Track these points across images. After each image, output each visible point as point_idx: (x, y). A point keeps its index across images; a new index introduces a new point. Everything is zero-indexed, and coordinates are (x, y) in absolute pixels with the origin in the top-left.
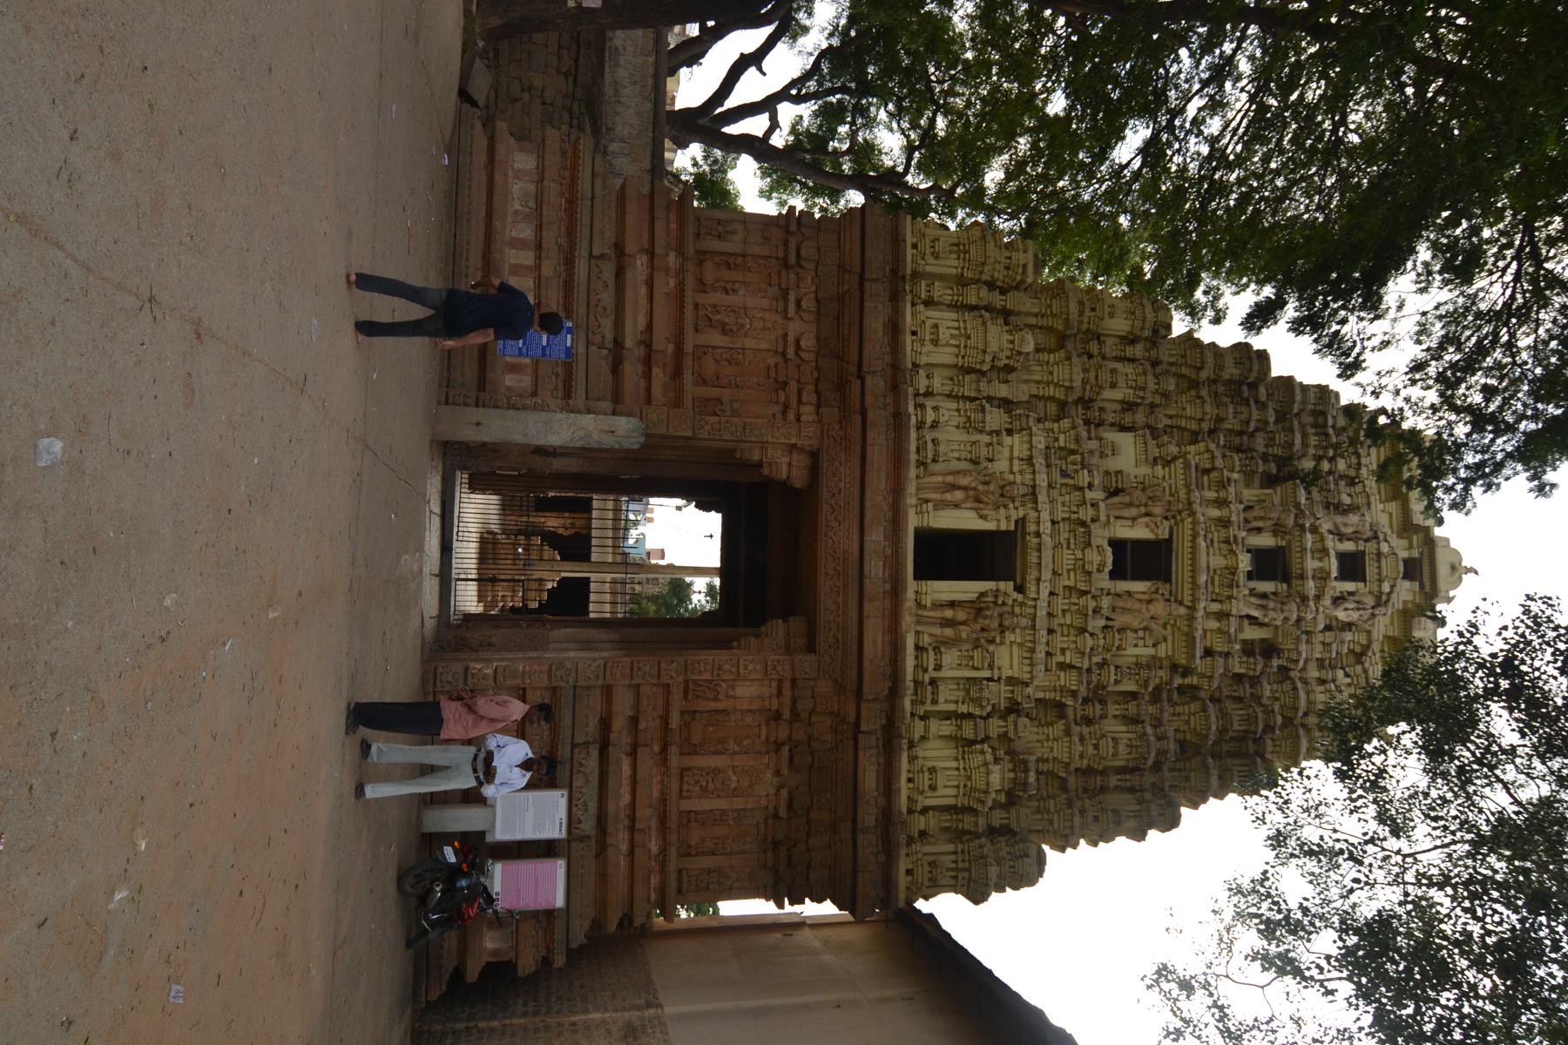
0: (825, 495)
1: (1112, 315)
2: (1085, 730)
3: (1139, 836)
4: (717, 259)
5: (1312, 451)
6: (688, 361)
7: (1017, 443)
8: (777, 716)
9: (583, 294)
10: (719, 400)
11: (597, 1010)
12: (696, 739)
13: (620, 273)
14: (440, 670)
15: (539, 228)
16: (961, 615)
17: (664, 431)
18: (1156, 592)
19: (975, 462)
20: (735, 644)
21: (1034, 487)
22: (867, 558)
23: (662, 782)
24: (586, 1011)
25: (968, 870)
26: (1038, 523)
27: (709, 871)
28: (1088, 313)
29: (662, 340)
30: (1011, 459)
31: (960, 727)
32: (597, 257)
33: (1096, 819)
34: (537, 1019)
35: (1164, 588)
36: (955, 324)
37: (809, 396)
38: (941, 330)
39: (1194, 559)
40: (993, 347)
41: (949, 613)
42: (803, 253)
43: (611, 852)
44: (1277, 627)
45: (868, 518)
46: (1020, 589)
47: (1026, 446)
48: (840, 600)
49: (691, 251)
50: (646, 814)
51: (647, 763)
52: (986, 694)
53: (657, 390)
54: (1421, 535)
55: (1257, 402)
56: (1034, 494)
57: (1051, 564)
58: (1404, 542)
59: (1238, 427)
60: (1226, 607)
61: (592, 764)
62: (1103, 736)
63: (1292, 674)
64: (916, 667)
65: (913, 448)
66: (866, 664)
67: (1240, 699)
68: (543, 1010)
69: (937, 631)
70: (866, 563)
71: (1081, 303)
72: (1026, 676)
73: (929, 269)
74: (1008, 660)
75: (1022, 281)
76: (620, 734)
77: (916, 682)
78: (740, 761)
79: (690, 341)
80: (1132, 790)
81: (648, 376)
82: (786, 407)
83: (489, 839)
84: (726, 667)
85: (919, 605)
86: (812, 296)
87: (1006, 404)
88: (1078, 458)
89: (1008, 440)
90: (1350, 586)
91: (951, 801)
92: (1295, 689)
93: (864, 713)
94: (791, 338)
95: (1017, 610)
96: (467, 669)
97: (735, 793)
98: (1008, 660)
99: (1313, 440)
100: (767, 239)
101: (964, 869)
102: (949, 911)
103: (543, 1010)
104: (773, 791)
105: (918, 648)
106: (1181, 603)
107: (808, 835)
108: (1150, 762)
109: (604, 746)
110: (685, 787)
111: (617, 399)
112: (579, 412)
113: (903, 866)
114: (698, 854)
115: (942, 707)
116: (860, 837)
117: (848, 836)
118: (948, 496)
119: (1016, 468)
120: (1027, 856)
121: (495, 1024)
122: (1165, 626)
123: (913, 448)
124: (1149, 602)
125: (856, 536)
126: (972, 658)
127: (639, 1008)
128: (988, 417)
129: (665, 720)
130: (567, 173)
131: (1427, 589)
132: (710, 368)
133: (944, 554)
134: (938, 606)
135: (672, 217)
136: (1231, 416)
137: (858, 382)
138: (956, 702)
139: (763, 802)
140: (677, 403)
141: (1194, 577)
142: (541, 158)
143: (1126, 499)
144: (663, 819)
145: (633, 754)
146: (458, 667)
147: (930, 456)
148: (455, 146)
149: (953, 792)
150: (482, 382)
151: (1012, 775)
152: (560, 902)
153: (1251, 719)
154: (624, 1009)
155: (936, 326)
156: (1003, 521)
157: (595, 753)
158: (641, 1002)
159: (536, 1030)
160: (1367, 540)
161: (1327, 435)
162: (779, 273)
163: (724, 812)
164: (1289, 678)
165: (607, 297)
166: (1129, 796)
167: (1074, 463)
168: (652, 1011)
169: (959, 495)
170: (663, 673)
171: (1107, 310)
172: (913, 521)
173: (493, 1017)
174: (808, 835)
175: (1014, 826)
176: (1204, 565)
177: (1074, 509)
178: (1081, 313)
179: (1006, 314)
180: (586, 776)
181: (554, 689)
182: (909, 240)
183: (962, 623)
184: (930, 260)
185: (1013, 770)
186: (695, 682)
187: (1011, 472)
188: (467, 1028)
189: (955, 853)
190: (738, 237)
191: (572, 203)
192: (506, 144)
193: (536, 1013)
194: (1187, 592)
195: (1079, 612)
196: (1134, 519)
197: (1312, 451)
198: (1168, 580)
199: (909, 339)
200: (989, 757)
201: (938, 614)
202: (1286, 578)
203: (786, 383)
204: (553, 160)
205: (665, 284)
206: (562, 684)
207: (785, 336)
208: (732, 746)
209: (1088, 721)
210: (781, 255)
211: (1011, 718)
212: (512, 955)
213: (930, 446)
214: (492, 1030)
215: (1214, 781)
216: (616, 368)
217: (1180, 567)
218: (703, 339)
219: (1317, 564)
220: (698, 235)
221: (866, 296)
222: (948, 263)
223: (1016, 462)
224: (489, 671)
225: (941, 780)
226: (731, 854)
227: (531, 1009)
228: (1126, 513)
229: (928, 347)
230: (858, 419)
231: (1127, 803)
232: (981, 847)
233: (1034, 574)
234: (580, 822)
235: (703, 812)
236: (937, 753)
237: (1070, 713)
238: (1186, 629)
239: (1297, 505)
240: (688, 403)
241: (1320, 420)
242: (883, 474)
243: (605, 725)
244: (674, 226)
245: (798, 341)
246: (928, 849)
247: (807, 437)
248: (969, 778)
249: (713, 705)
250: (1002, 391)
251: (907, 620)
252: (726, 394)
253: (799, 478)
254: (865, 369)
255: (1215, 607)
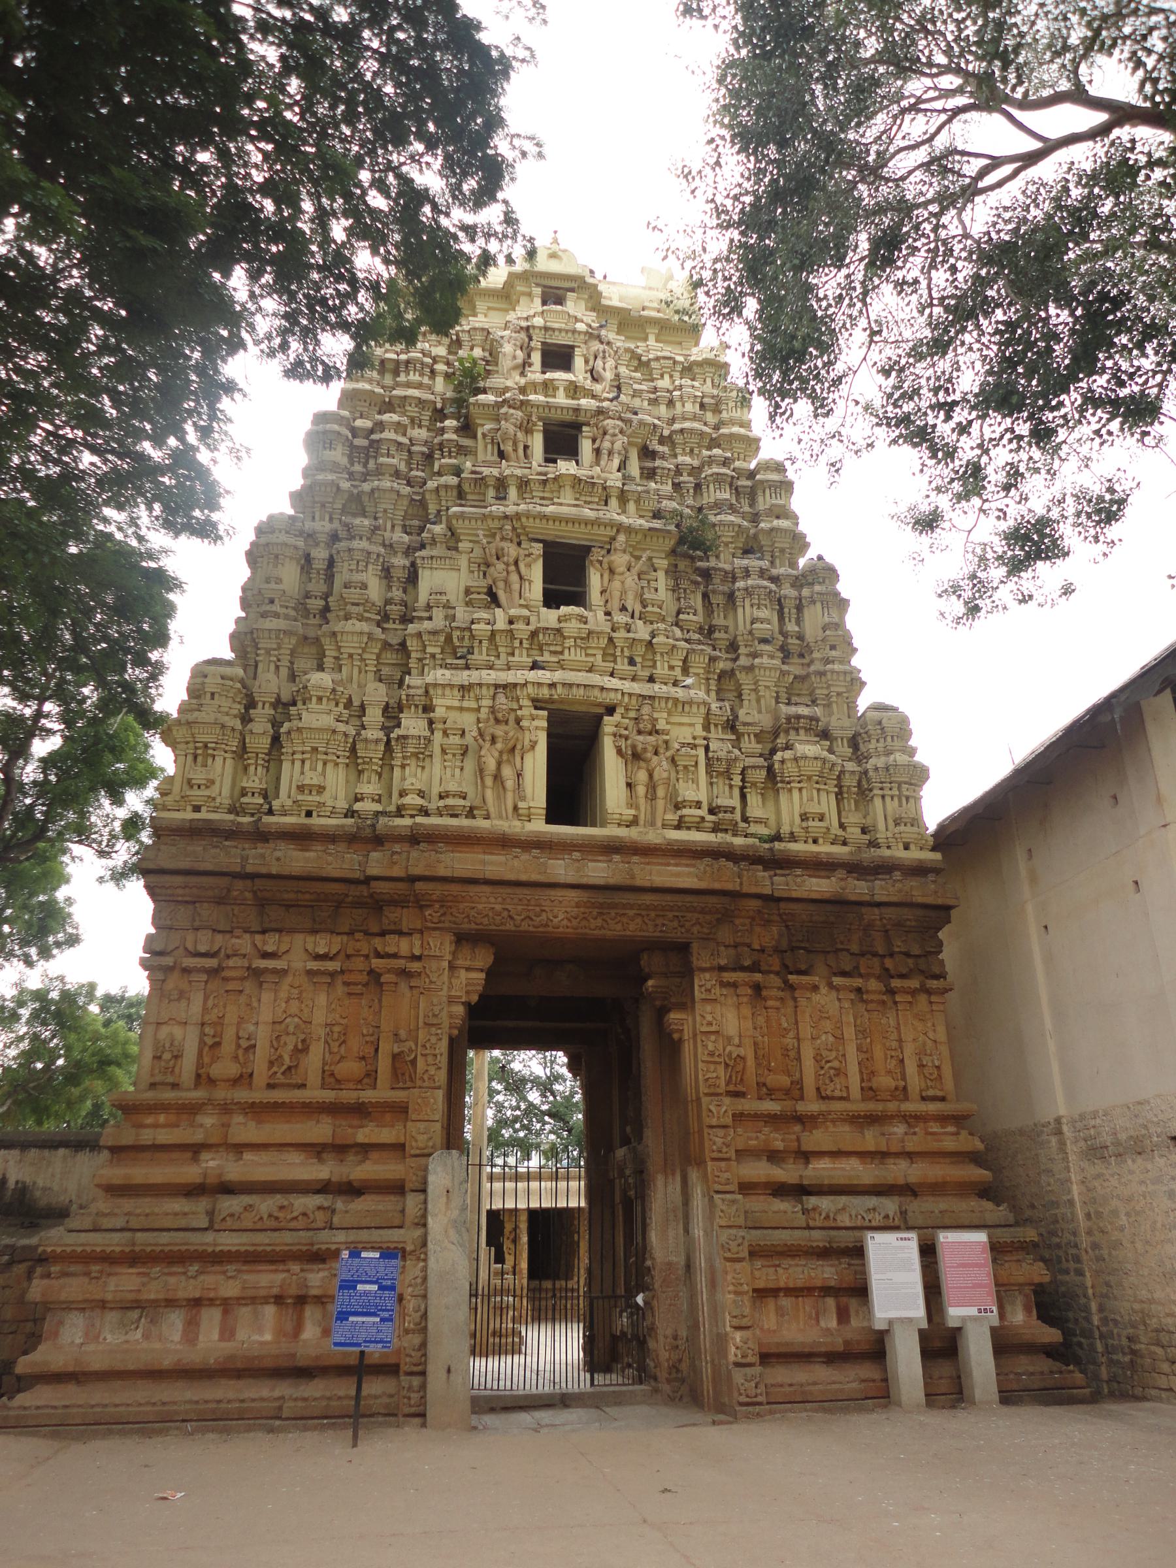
0: (510, 926)
1: (279, 581)
2: (742, 650)
3: (843, 604)
4: (206, 1060)
5: (426, 380)
6: (348, 1096)
7: (442, 704)
8: (757, 988)
9: (261, 1238)
10: (395, 1057)
11: (1069, 1192)
12: (785, 1081)
13: (228, 1189)
14: (743, 1399)
15: (171, 1303)
16: (642, 776)
17: (438, 1126)
18: (601, 562)
19: (465, 751)
20: (676, 1036)
21: (496, 686)
22: (584, 881)
23: (833, 1121)
24: (1071, 1202)
25: (900, 784)
26: (540, 684)
27: (921, 1066)
28: (276, 608)
29: (321, 1130)
30: (461, 709)
31: (754, 784)
32: (211, 1221)
33: (833, 647)
34: (1085, 1257)
35: (596, 554)
36: (298, 764)
37: (392, 944)
38: (307, 782)
39: (568, 520)
40: (328, 721)
41: (641, 790)
42: (202, 949)
43: (912, 1179)
44: (630, 443)
45: (535, 877)
46: (611, 710)
47: (448, 691)
48: (631, 913)
49: (199, 1094)
50: (870, 1139)
51: (817, 1139)
52: (722, 754)
53: (386, 1135)
54: (517, 282)
55: (372, 431)
56: (505, 687)
57: (580, 678)
58: (523, 300)
59: (405, 455)
60: (614, 493)
61: (825, 1203)
62: (751, 633)
63: (666, 433)
64: (698, 829)
65: (454, 822)
66: (703, 885)
67: (698, 487)
68: (1073, 1251)
69: (660, 804)
70: (591, 881)
71: (264, 615)
72: (703, 710)
73: (226, 791)
74: (683, 730)
75: (242, 681)
76: (786, 1173)
77: (715, 830)
78: (806, 1030)
79: (315, 1094)
80: (799, 608)
81: (366, 1149)
82: (404, 973)
83: (924, 1325)
84: (711, 1047)
85: (634, 822)
86: (258, 937)
87: (392, 714)
88: (456, 634)
89: (440, 712)
90: (578, 362)
91: (833, 797)
92: (682, 431)
93: (754, 890)
94: (313, 965)
95: (632, 714)
96: (737, 1365)
97: (840, 1039)
98: (683, 730)
99: (414, 377)
100: (182, 995)
101: (899, 788)
102: (938, 805)
103: (1073, 1251)
104: (834, 994)
105: (678, 827)
106: (614, 539)
107: (875, 955)
108: (773, 587)
109: (800, 1191)
110: (837, 1093)
111: (397, 1188)
112: (426, 1235)
113: (899, 853)
114: (904, 1078)
115: (735, 802)
116: (877, 898)
117: (876, 910)
118: (510, 784)
119: (474, 705)
120: (880, 723)
121: (1094, 1307)
122: (638, 558)
123: (454, 822)
124: (612, 571)
125: (559, 893)
126: (685, 767)
127: (1062, 1144)
128: (412, 732)
129: (772, 1119)
130: (95, 1268)
131: (573, 285)
132: (352, 1067)
133: (571, 792)
134: (632, 803)
135: (149, 1120)
136: (390, 461)
137: (373, 884)
138: (731, 786)
139: (847, 1005)
140: (401, 1111)
141: (586, 522)
142: (69, 1306)
143: (501, 584)
144: (872, 1119)
145: (806, 1156)
146: (738, 1376)
147: (462, 802)
148: (64, 1428)
149: (823, 795)
150: (389, 1369)
151: (802, 732)
152: (981, 1237)
153: (719, 479)
154: (1066, 1159)
155: (301, 788)
156: (536, 723)
157: (812, 1201)
158: (1054, 1140)
159: (1100, 1259)
160: (530, 339)
161: (408, 362)
162: (226, 979)
163: (859, 1049)
164: (670, 436)
165: (266, 1205)
166: (806, 611)
167: (461, 639)
168: (1065, 1128)
169: (507, 772)
170: (723, 1121)
171: (273, 586)
172: (539, 826)
173: (1086, 1309)
174: (875, 955)
175: (850, 734)
176: (574, 510)
177: (517, 643)
178: (277, 615)
179: (284, 707)
180: (839, 1211)
181: (752, 1254)
182: (190, 815)
183: (651, 776)
184: (213, 791)
185: (797, 730)
186: (728, 1083)
187: (478, 710)
188: (1102, 1337)
189: (883, 797)
190: (178, 1032)
191: (133, 1259)
192: (45, 1356)
193: (1077, 1259)
194: (602, 531)
195: (630, 647)
196: (521, 578)
197: (426, 380)
198: (587, 549)
199: (315, 821)
200: (788, 754)
201: (642, 801)
202: (577, 427)
203: (371, 972)
204: (74, 1288)
205: (245, 1130)
206: (746, 1244)
207: (310, 973)
208: (789, 1041)
209: (733, 647)
210: (204, 977)
211: (741, 729)
212: (1027, 1290)
213: (450, 801)
214: (1101, 1309)
215: (783, 523)
216: (352, 1190)
217: (574, 536)
218: (314, 1078)
219: (561, 393)
220: (175, 1086)
221: (264, 870)
222: (219, 769)
223: (466, 704)
224: (738, 1336)
225: (814, 808)
226: (900, 1041)
227: (1072, 1265)
228: (516, 587)
229: (326, 797)
230: (419, 885)
231: (814, 618)
232: (876, 769)
233: (596, 692)
234: (887, 1217)
235: (861, 1072)
236: (789, 809)
237: (728, 665)
238: (640, 537)
239: (499, 405)
240: (399, 1096)
241: (389, 366)
242: (487, 857)
243: (780, 1190)
244: (162, 1118)
245: (318, 957)
246: (881, 825)
247: (441, 945)
248: (809, 778)
249: (751, 1062)
250: (374, 715)
251: (653, 836)
252: (387, 1048)
253: (484, 958)
254: (357, 875)
255: (614, 502)
